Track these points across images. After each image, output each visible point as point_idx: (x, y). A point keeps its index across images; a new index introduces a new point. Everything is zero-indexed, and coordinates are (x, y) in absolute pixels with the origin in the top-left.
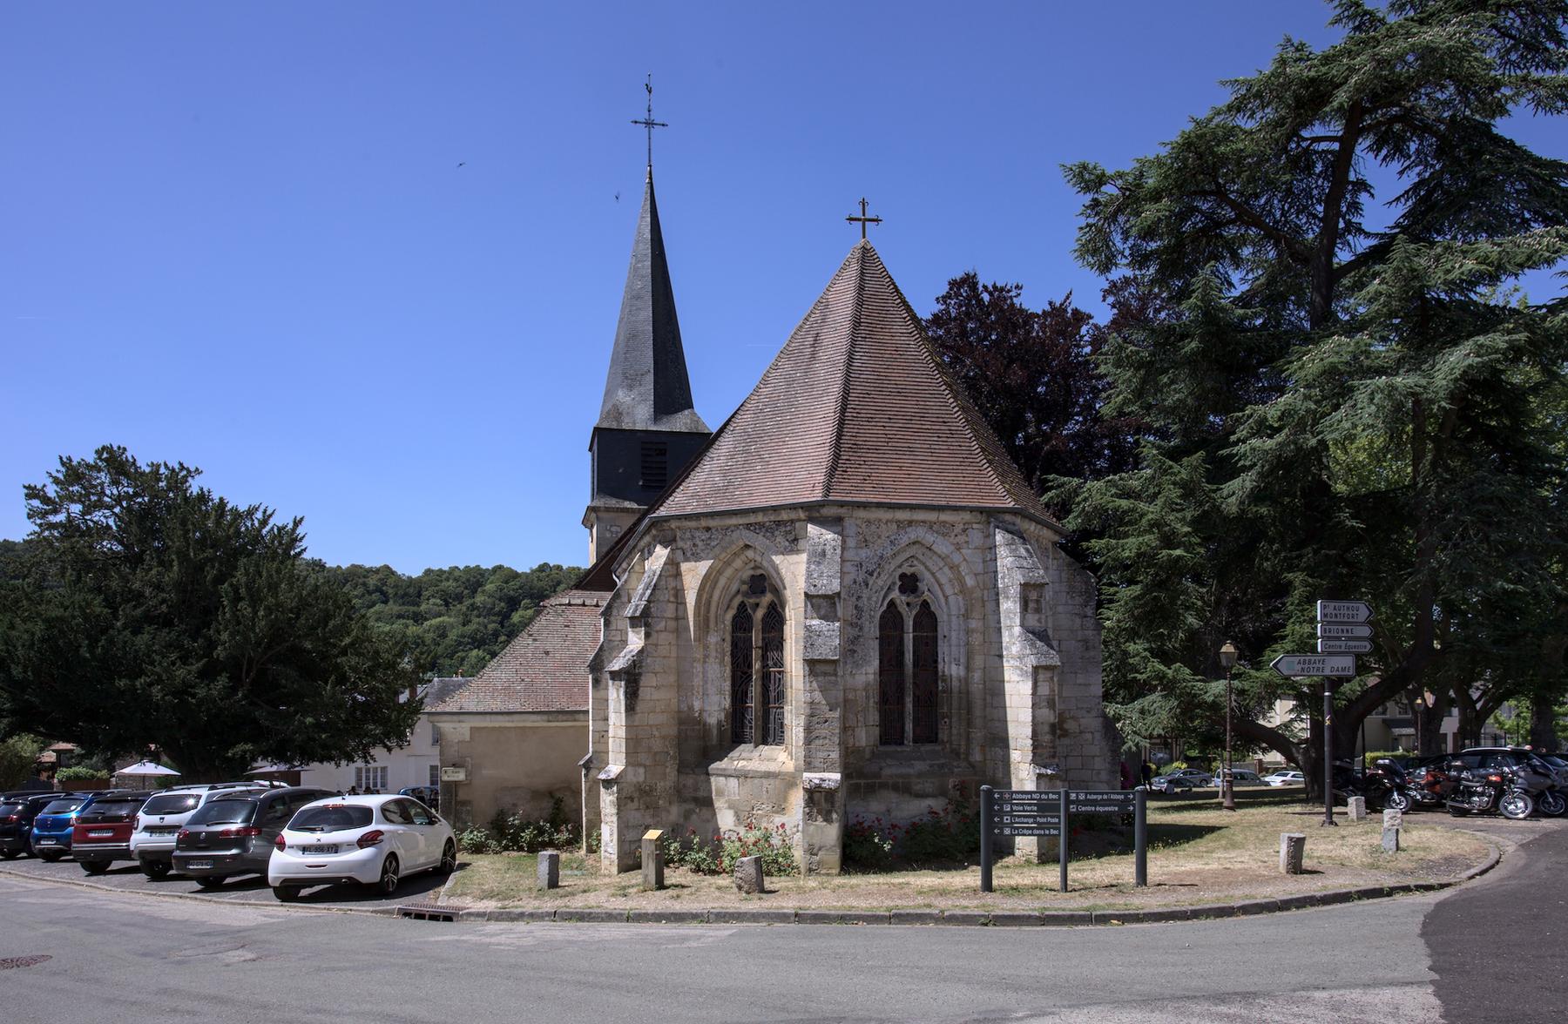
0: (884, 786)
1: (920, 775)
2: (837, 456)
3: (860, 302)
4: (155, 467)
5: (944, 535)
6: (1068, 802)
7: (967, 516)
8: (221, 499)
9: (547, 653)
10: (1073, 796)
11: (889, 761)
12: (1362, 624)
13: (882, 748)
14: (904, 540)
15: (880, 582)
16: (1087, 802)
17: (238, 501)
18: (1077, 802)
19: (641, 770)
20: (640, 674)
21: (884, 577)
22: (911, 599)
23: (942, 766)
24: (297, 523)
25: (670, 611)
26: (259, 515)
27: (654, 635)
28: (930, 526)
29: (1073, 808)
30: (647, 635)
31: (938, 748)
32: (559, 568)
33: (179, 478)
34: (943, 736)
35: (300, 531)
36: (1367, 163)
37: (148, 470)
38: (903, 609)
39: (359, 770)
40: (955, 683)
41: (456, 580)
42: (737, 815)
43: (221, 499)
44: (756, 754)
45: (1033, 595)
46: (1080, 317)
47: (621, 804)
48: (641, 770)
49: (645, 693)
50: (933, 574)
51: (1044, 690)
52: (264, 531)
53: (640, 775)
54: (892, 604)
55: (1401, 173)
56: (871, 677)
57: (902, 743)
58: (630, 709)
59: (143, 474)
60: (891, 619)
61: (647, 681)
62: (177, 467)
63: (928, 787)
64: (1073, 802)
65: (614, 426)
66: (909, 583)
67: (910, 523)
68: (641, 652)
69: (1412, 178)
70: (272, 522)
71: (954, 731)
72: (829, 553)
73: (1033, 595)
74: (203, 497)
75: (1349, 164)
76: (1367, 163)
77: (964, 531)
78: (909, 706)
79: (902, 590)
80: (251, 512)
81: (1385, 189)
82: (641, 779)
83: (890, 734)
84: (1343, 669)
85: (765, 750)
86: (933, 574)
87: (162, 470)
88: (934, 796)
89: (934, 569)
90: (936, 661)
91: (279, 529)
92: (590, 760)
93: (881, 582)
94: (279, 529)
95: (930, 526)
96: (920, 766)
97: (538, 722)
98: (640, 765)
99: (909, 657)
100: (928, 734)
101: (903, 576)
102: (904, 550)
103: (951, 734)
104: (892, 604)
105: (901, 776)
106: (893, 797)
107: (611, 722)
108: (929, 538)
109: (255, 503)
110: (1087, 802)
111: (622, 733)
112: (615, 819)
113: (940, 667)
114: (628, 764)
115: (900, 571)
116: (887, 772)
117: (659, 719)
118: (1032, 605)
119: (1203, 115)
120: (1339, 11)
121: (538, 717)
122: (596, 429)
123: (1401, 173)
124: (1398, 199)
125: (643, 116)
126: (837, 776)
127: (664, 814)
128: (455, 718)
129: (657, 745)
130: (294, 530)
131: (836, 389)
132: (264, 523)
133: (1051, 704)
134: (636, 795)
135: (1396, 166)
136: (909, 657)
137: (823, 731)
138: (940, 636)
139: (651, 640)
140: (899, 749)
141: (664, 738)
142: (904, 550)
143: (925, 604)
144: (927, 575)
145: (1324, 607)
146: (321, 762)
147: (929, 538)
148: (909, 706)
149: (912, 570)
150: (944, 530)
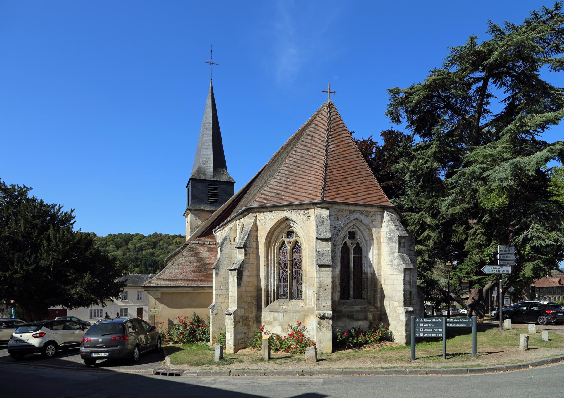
0: (343, 316)
1: (357, 311)
2: (325, 183)
3: (330, 123)
4: (13, 186)
5: (367, 216)
6: (446, 322)
7: (376, 209)
8: (42, 200)
9: (191, 263)
10: (448, 320)
11: (345, 306)
12: (512, 254)
13: (342, 301)
14: (352, 218)
15: (342, 235)
16: (453, 323)
17: (48, 201)
18: (450, 322)
19: (243, 310)
20: (243, 271)
21: (343, 232)
22: (353, 241)
23: (365, 308)
24: (72, 211)
25: (254, 245)
26: (57, 207)
27: (248, 255)
28: (362, 212)
29: (448, 325)
30: (246, 255)
31: (363, 301)
32: (161, 234)
33: (23, 192)
34: (364, 296)
35: (73, 214)
36: (492, 88)
37: (9, 187)
38: (349, 245)
39: (91, 310)
40: (369, 275)
41: (121, 239)
42: (283, 328)
43: (42, 200)
44: (290, 303)
45: (403, 241)
46: (373, 143)
47: (236, 323)
48: (243, 310)
49: (244, 278)
50: (361, 232)
51: (408, 278)
52: (59, 213)
53: (242, 312)
54: (345, 243)
55: (505, 92)
56: (338, 272)
57: (349, 299)
58: (239, 284)
59: (8, 189)
60: (345, 249)
61: (246, 273)
62: (22, 187)
63: (360, 316)
64: (448, 322)
65: (198, 178)
66: (352, 235)
67: (354, 211)
68: (243, 261)
69: (509, 94)
70: (62, 210)
71: (369, 294)
72: (325, 222)
73: (403, 241)
74: (34, 200)
75: (486, 89)
76: (492, 88)
77: (374, 215)
78: (352, 284)
79: (350, 238)
80: (53, 207)
81: (498, 99)
82: (243, 314)
83: (344, 294)
84: (507, 271)
85: (293, 301)
86: (361, 232)
87: (16, 187)
88: (362, 320)
89: (362, 230)
90: (361, 267)
91: (65, 213)
92: (214, 306)
93: (342, 234)
94: (65, 213)
95: (362, 212)
96: (357, 308)
97: (190, 290)
98: (242, 308)
99: (352, 265)
100: (358, 295)
101: (350, 232)
102: (351, 222)
103: (367, 295)
104: (345, 243)
105: (350, 312)
106: (347, 320)
107: (230, 290)
108: (361, 217)
109: (55, 203)
110: (453, 323)
111: (236, 295)
112: (233, 330)
113: (363, 269)
114: (238, 307)
115: (349, 230)
116: (345, 310)
117: (251, 289)
118: (402, 244)
119: (440, 66)
120: (489, 28)
121: (189, 289)
122: (190, 179)
123: (505, 92)
124: (502, 101)
125: (209, 60)
126: (331, 312)
127: (251, 328)
128: (155, 289)
129: (249, 300)
130: (71, 213)
131: (323, 157)
132: (59, 210)
133: (410, 283)
134: (241, 320)
135: (503, 89)
136: (352, 265)
137: (324, 294)
138: (363, 256)
139: (247, 257)
140: (348, 301)
141: (252, 297)
142: (351, 222)
143: (358, 244)
144: (359, 232)
145: (500, 248)
146: (84, 307)
147: (361, 217)
148: (352, 284)
149: (354, 230)
150: (367, 214)
